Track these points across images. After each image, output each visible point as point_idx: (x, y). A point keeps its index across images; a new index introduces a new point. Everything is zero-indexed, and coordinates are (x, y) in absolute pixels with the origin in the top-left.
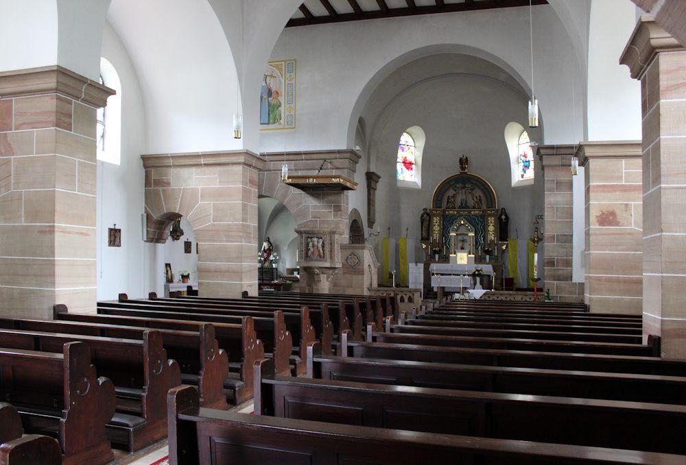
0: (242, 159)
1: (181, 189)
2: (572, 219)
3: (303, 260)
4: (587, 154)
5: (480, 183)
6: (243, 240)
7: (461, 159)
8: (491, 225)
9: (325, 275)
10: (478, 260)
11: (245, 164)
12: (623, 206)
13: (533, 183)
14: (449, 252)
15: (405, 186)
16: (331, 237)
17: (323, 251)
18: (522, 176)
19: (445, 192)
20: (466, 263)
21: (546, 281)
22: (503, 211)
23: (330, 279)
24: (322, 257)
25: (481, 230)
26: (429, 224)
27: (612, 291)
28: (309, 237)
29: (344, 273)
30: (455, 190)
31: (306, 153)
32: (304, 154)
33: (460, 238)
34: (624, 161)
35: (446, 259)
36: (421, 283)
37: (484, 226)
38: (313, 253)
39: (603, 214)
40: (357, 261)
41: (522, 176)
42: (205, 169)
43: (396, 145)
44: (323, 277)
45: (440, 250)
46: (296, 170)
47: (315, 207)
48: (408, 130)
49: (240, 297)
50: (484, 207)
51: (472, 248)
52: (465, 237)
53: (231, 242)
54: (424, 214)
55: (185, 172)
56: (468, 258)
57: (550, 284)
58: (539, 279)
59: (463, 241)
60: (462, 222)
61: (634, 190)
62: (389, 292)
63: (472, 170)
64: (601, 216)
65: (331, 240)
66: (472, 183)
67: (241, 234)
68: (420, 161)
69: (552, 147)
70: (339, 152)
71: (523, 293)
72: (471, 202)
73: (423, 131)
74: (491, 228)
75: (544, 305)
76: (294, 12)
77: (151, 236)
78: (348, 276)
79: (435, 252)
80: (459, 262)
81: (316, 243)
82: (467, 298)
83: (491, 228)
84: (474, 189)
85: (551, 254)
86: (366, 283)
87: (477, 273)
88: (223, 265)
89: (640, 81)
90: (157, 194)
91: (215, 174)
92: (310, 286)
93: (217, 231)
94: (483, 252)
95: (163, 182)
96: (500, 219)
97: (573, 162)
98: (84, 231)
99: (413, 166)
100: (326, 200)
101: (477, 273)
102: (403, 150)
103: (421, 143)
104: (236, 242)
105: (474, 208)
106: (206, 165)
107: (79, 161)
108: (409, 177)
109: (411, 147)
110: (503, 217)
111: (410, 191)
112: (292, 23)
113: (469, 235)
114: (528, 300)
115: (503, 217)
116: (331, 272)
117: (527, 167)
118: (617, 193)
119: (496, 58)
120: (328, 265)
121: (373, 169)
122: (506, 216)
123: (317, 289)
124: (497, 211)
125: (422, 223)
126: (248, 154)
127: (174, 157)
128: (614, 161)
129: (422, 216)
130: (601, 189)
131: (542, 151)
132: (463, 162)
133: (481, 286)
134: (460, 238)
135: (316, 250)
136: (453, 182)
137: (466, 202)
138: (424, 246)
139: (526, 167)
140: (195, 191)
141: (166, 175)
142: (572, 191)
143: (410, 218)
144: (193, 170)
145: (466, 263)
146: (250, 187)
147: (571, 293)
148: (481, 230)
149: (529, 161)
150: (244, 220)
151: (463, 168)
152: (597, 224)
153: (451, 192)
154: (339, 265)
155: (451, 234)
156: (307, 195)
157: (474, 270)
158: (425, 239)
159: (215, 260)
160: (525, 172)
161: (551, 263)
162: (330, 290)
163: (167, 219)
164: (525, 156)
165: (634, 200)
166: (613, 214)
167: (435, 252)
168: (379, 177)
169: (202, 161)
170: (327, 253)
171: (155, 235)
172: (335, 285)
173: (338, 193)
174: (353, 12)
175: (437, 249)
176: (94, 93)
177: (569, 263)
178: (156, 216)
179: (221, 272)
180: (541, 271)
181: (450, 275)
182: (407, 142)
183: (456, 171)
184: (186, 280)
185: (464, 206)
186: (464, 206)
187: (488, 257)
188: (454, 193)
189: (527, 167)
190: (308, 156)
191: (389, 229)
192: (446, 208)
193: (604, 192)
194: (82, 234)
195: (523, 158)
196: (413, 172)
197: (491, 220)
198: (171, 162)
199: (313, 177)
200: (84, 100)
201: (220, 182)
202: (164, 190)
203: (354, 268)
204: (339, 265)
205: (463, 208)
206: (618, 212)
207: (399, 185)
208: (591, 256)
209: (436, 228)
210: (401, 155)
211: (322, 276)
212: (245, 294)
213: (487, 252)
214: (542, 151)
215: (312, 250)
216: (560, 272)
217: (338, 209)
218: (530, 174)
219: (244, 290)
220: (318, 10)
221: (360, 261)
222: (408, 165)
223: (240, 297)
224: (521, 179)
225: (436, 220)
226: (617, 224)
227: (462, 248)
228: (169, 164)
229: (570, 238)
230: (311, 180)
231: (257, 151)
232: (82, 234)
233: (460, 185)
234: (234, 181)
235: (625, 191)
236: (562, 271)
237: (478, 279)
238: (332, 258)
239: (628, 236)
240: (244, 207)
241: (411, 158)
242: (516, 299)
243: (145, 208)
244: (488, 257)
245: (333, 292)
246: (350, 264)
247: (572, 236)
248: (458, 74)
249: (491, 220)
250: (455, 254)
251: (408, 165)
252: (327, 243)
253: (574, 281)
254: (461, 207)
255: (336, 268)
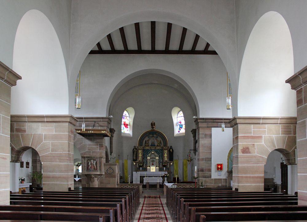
0: (68, 120)
1: (32, 134)
2: (211, 150)
3: (86, 171)
4: (237, 122)
5: (143, 136)
6: (69, 161)
7: (152, 124)
8: (166, 153)
9: (97, 178)
10: (161, 170)
11: (70, 122)
12: (252, 145)
13: (184, 134)
14: (147, 167)
15: (124, 135)
16: (100, 159)
17: (96, 166)
18: (179, 132)
19: (144, 139)
20: (151, 171)
21: (200, 179)
22: (171, 147)
23: (99, 180)
24: (96, 169)
25: (162, 157)
26: (136, 154)
27: (254, 182)
28: (89, 160)
29: (106, 177)
30: (149, 138)
31: (85, 118)
32: (84, 118)
33: (152, 160)
34: (252, 125)
35: (145, 170)
36: (134, 181)
37: (162, 154)
38: (91, 167)
39: (244, 148)
40: (112, 171)
41: (179, 132)
42: (47, 124)
43: (121, 117)
44: (96, 179)
45: (142, 165)
46: (79, 126)
47: (90, 145)
48: (127, 109)
49: (67, 191)
50: (162, 145)
51: (158, 164)
52: (154, 159)
53: (62, 162)
54: (134, 148)
55: (34, 125)
56: (156, 169)
57: (202, 179)
58: (197, 178)
59: (153, 161)
60: (153, 153)
61: (257, 138)
62: (128, 186)
63: (156, 129)
64: (243, 149)
65: (100, 161)
66: (157, 135)
67: (67, 158)
68: (132, 124)
69: (203, 119)
70: (102, 118)
71: (190, 184)
72: (156, 144)
73: (134, 110)
74: (166, 155)
75: (199, 189)
76: (94, 47)
77: (14, 159)
78: (107, 178)
79: (140, 166)
80: (152, 171)
81: (93, 163)
82: (174, 187)
83: (166, 155)
84: (158, 137)
85: (202, 166)
86: (114, 183)
87: (165, 175)
88: (57, 174)
89: (296, 91)
90: (18, 136)
91: (52, 127)
92: (88, 183)
93: (54, 156)
94: (162, 166)
95: (21, 130)
96: (169, 151)
97: (222, 126)
98: (4, 157)
99: (128, 126)
100: (95, 141)
101: (165, 175)
102: (124, 119)
103: (133, 116)
104: (65, 162)
105: (158, 146)
106: (47, 122)
107: (2, 116)
108: (127, 131)
109: (128, 117)
110: (171, 150)
111: (127, 138)
112: (92, 52)
113: (156, 158)
114: (192, 187)
115: (171, 150)
116: (99, 176)
117: (181, 128)
118: (250, 139)
119: (179, 77)
120: (99, 173)
121: (112, 127)
122: (172, 149)
123: (93, 185)
124: (168, 147)
125: (133, 153)
126: (72, 117)
127: (29, 117)
128: (249, 125)
129: (133, 149)
130: (243, 138)
131: (199, 121)
132: (153, 125)
133: (167, 182)
134: (152, 160)
135: (92, 166)
136: (157, 134)
137: (154, 143)
138: (134, 164)
139: (181, 127)
140: (40, 135)
141: (23, 126)
142: (211, 138)
143: (127, 150)
144: (40, 124)
145: (151, 171)
146: (71, 134)
147: (211, 183)
148: (162, 157)
149: (182, 125)
150: (69, 151)
151: (153, 128)
152: (241, 153)
153: (147, 139)
154: (104, 173)
155: (148, 158)
156: (85, 139)
157: (164, 174)
158: (134, 160)
159: (53, 172)
160: (180, 130)
161: (202, 170)
162: (98, 186)
163: (22, 150)
164: (180, 123)
165: (256, 142)
166: (248, 148)
167: (140, 166)
168: (115, 131)
169: (45, 120)
170: (98, 168)
171: (15, 158)
172: (101, 183)
173: (101, 139)
174: (111, 50)
175: (141, 165)
176: (11, 76)
177: (210, 170)
178: (17, 148)
179: (57, 178)
180: (198, 174)
181: (153, 177)
182: (125, 115)
183: (150, 129)
184: (23, 181)
185: (153, 145)
186: (153, 145)
187: (165, 168)
188: (148, 139)
189: (181, 128)
190: (86, 120)
191: (119, 156)
192: (145, 146)
193: (244, 139)
194: (3, 158)
195: (179, 124)
196: (128, 129)
197: (166, 152)
198: (27, 119)
199: (92, 130)
200: (6, 81)
201: (55, 131)
202: (21, 135)
203: (110, 174)
204: (104, 173)
205: (153, 146)
206: (250, 148)
207: (122, 135)
208: (239, 167)
209: (140, 155)
210: (123, 120)
211: (95, 178)
212: (70, 189)
213: (164, 166)
214: (199, 121)
215: (90, 166)
216: (206, 174)
217: (101, 146)
218: (183, 131)
219: (69, 187)
220: (106, 46)
221: (114, 171)
222: (126, 125)
223: (67, 191)
224: (178, 133)
225: (140, 151)
226: (250, 153)
227: (153, 165)
228: (26, 121)
229: (210, 159)
230: (91, 132)
231: (76, 115)
232: (3, 158)
233: (151, 135)
234: (64, 130)
235: (253, 138)
236: (207, 173)
237: (166, 178)
238: (100, 170)
239: (254, 158)
240: (69, 144)
241: (127, 122)
242: (187, 187)
243: (10, 143)
244: (165, 168)
245: (100, 187)
246: (109, 172)
247: (211, 158)
248: (155, 83)
249: (166, 152)
250: (149, 167)
251: (126, 125)
252: (98, 162)
253: (212, 178)
254: (152, 145)
255: (102, 175)
